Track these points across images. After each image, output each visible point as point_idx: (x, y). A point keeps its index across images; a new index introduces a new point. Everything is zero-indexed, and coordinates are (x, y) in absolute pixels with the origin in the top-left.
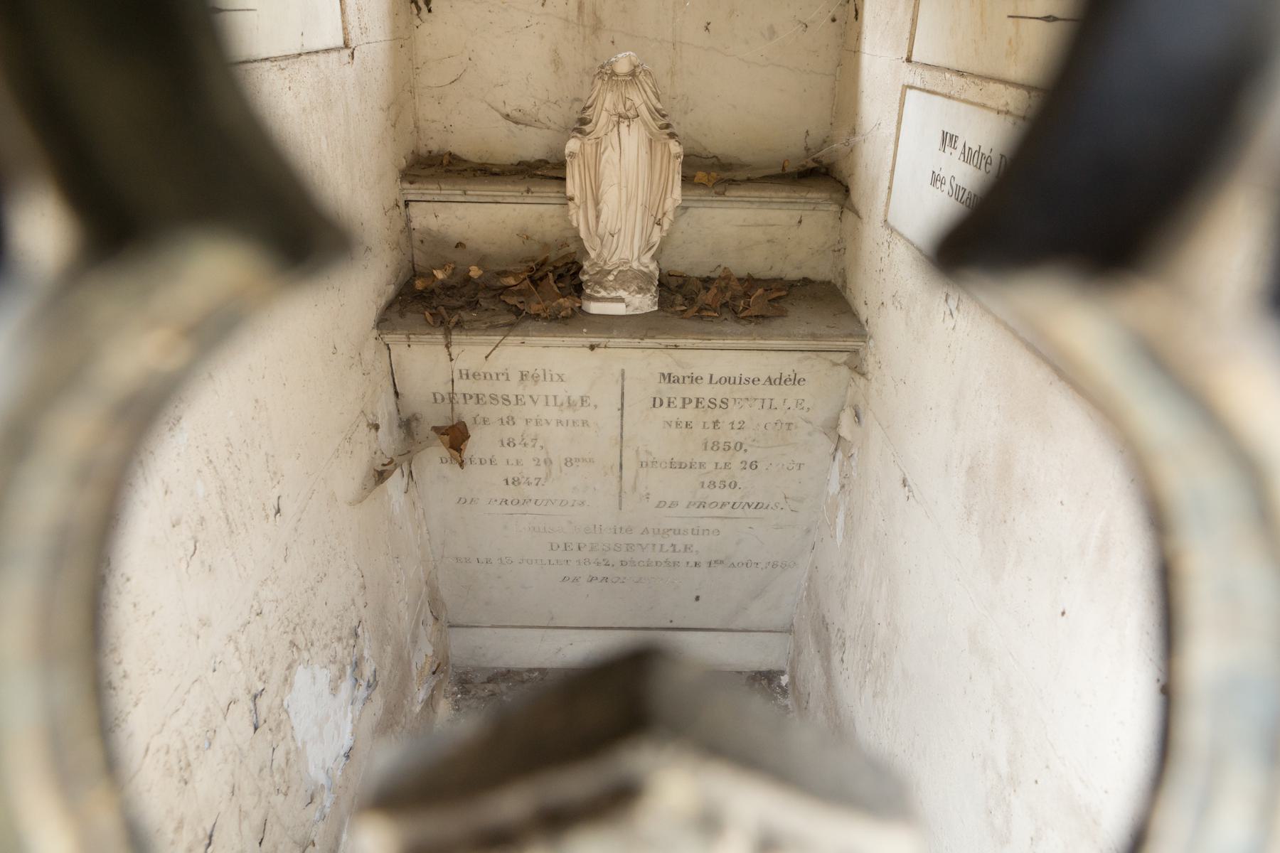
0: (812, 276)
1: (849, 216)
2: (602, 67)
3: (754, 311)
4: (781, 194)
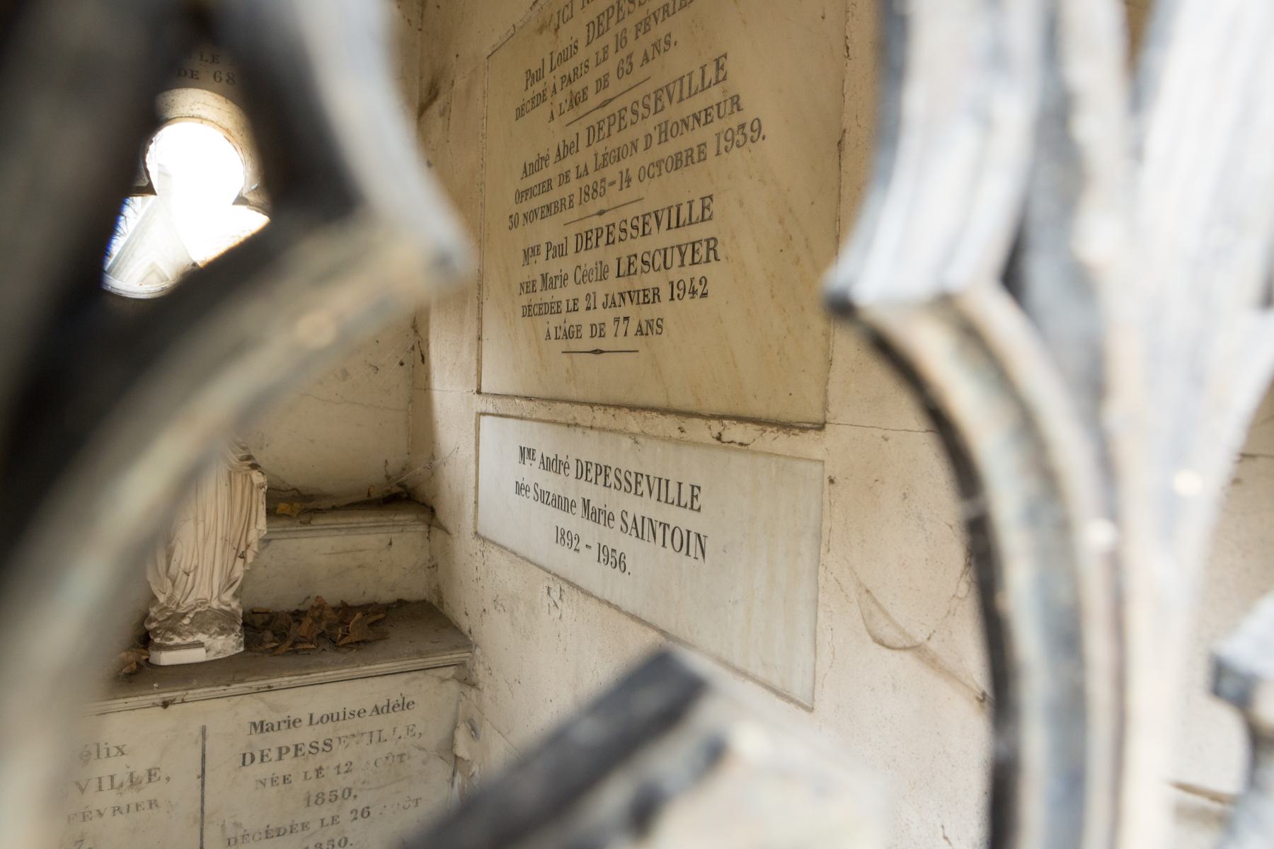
0: (406, 597)
1: (438, 535)
3: (354, 637)
4: (369, 519)
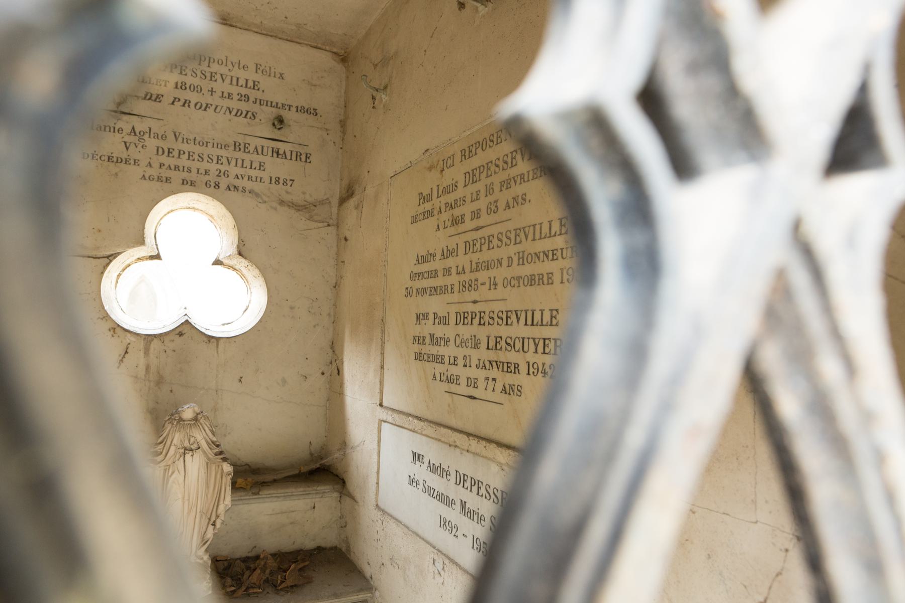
0: (323, 545)
3: (289, 582)
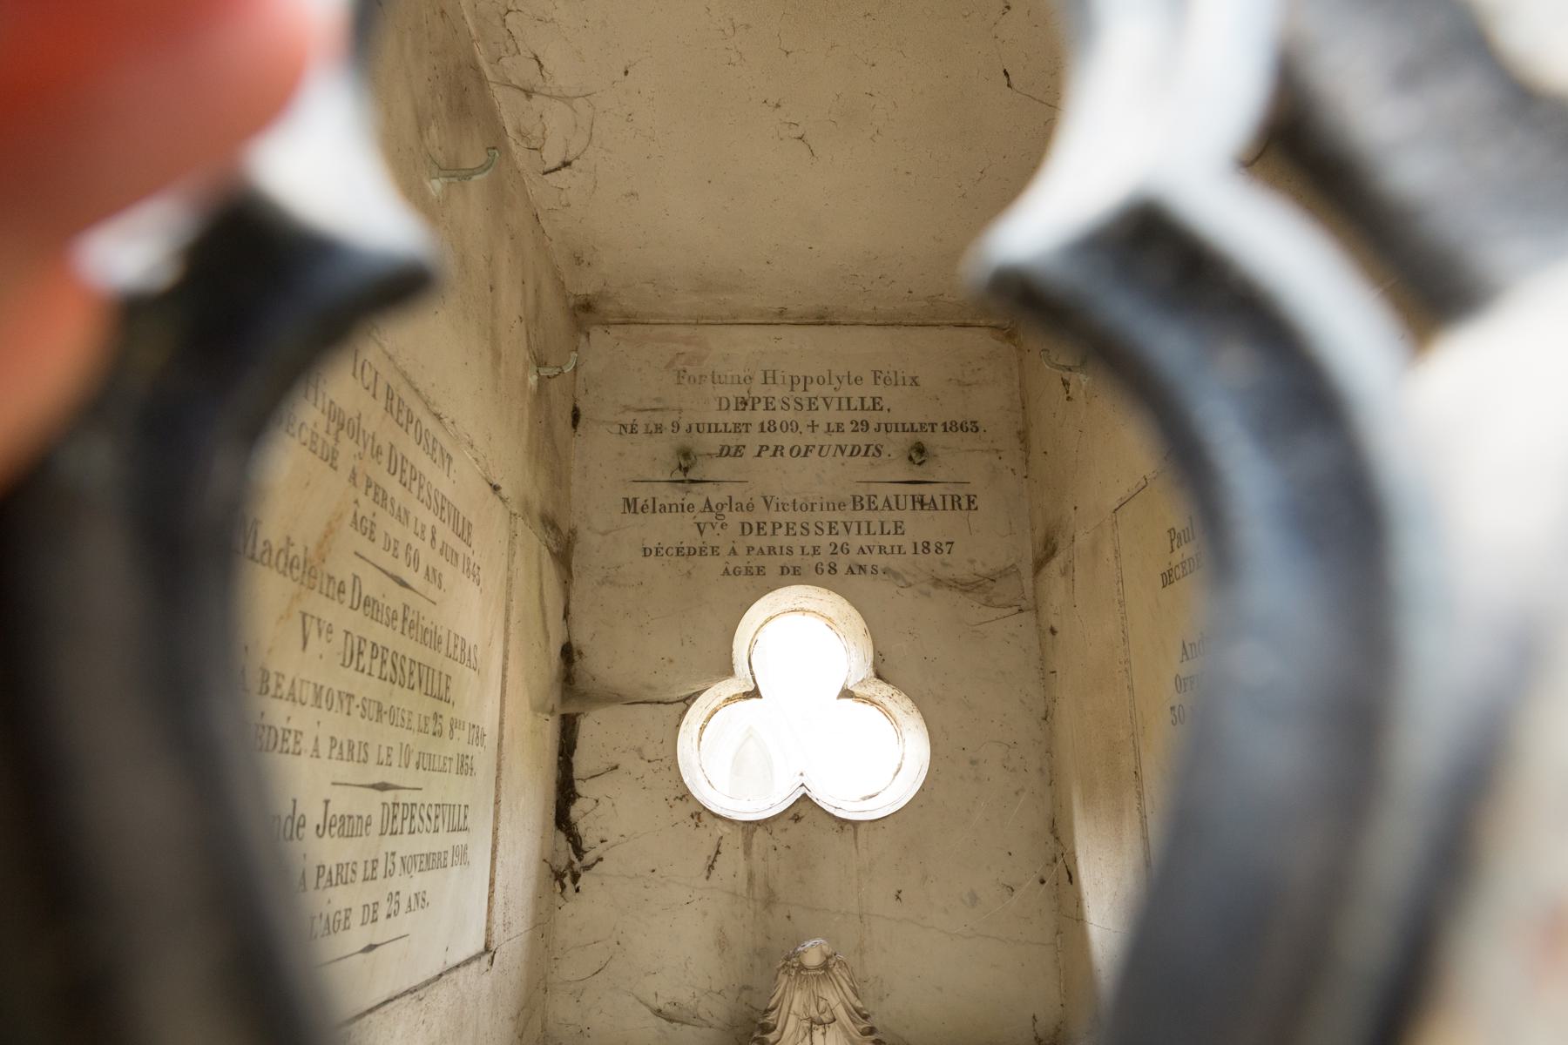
2: (788, 959)
